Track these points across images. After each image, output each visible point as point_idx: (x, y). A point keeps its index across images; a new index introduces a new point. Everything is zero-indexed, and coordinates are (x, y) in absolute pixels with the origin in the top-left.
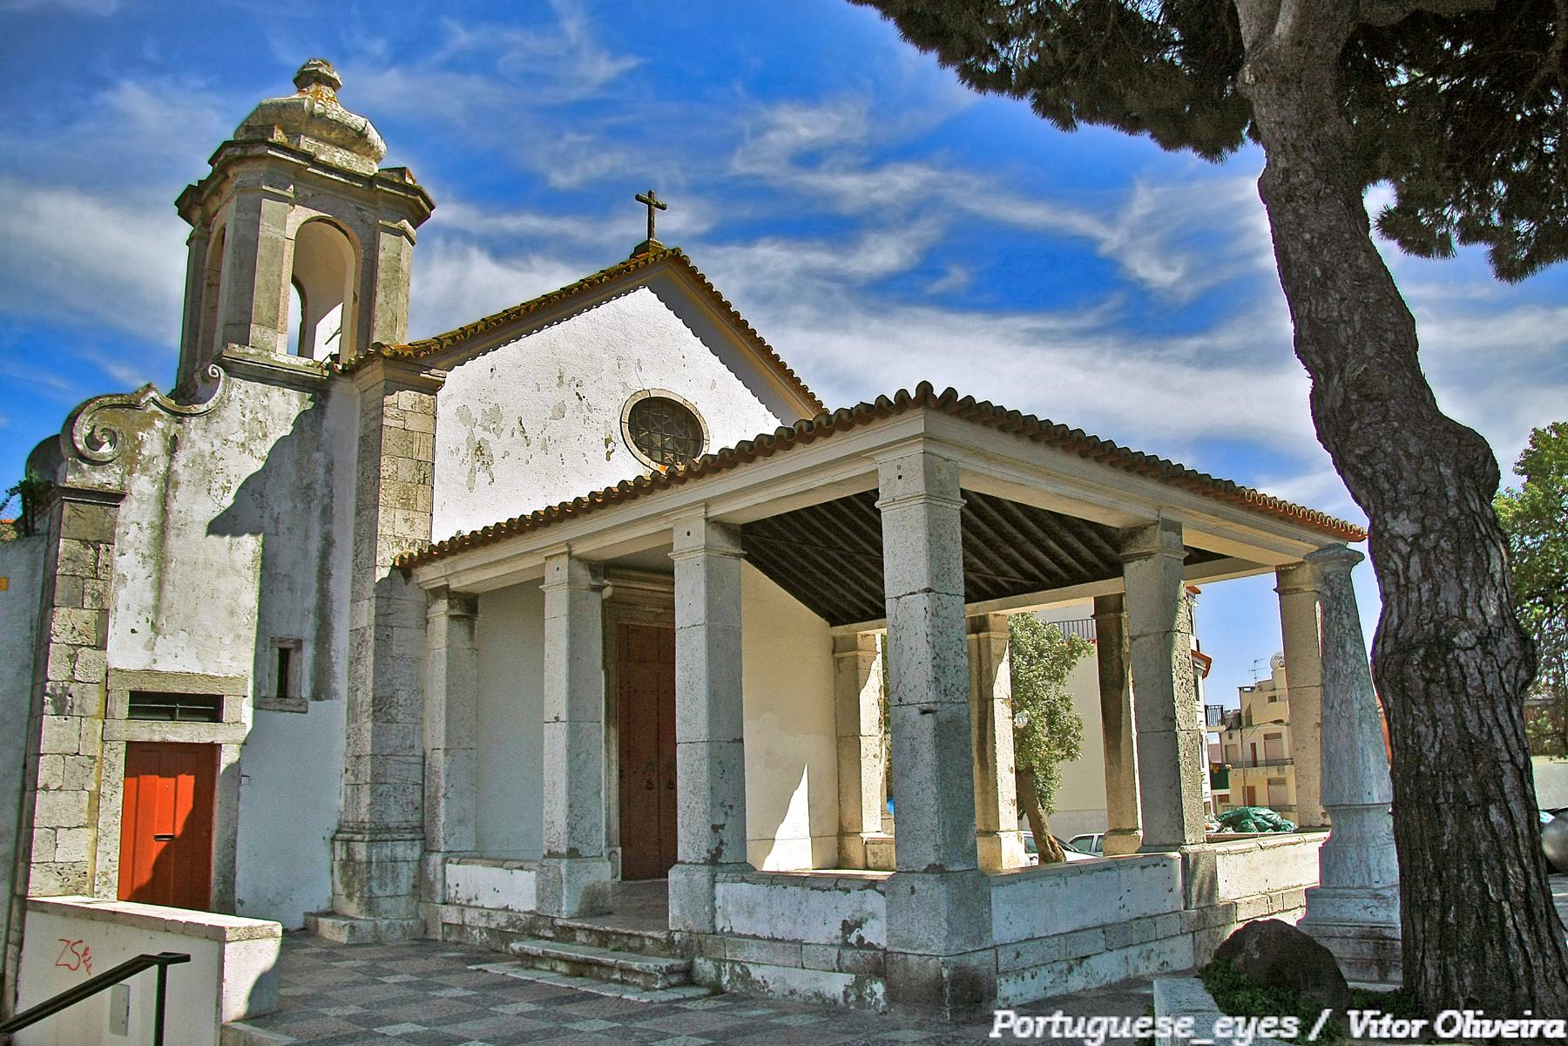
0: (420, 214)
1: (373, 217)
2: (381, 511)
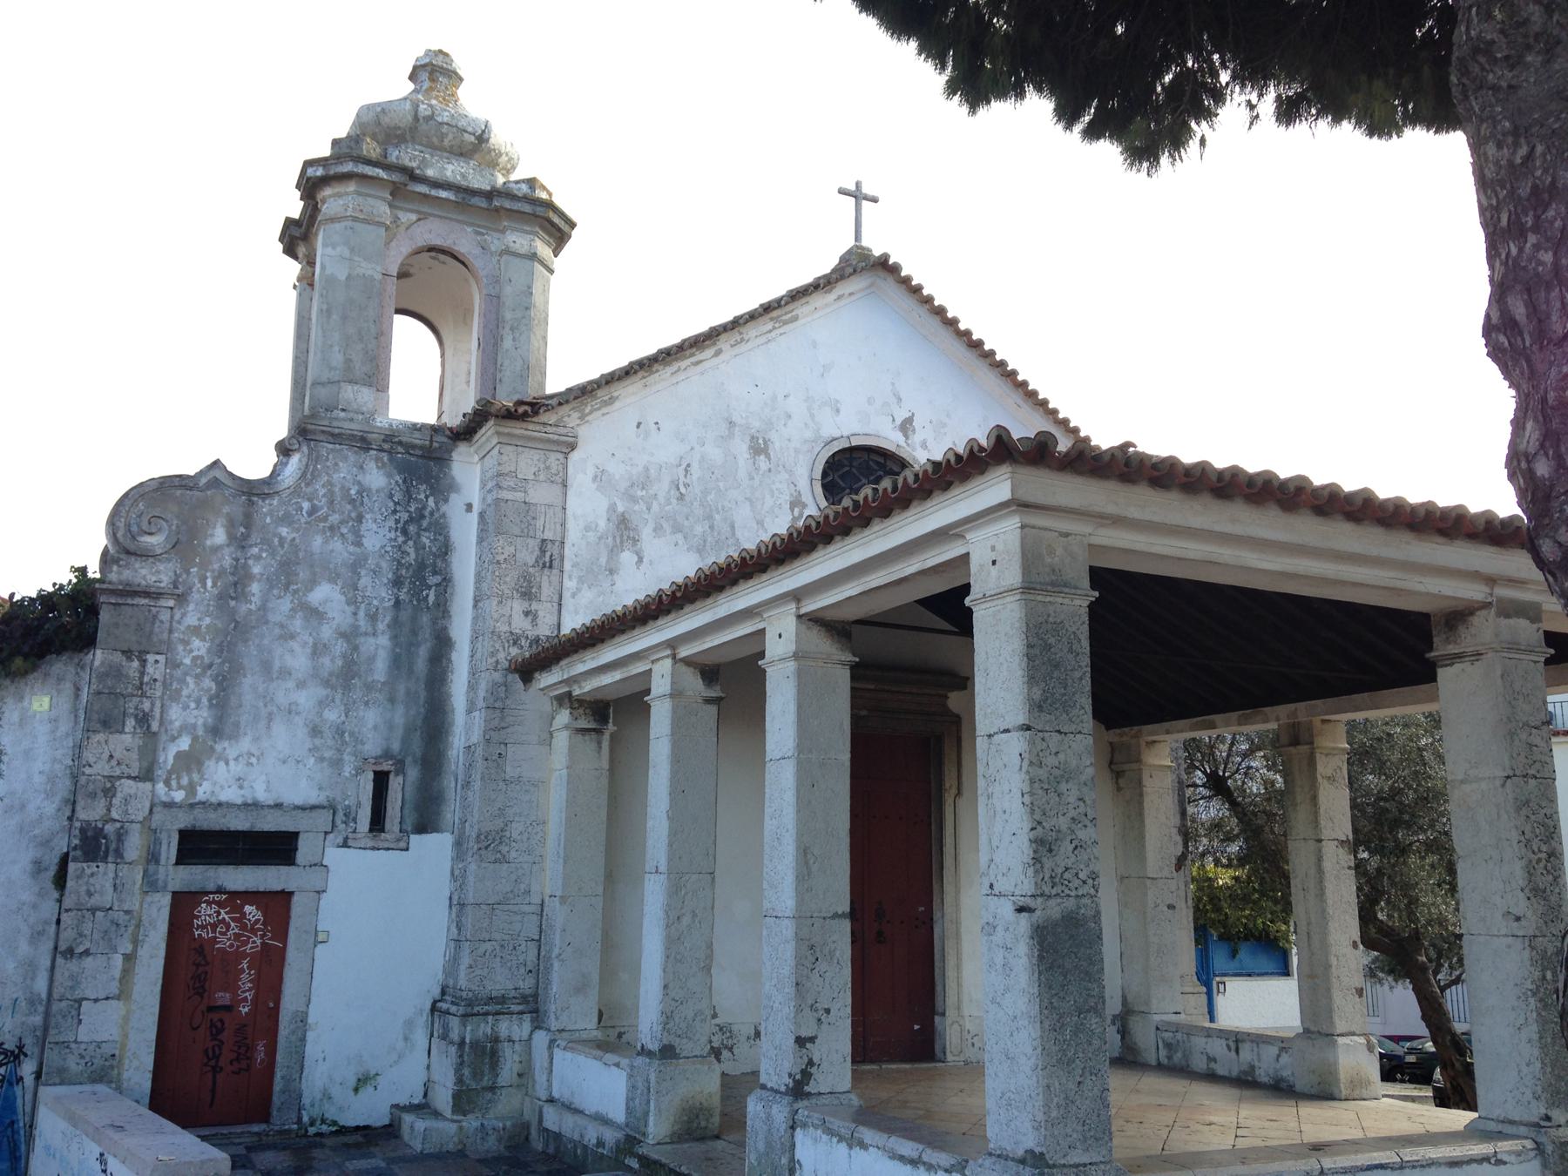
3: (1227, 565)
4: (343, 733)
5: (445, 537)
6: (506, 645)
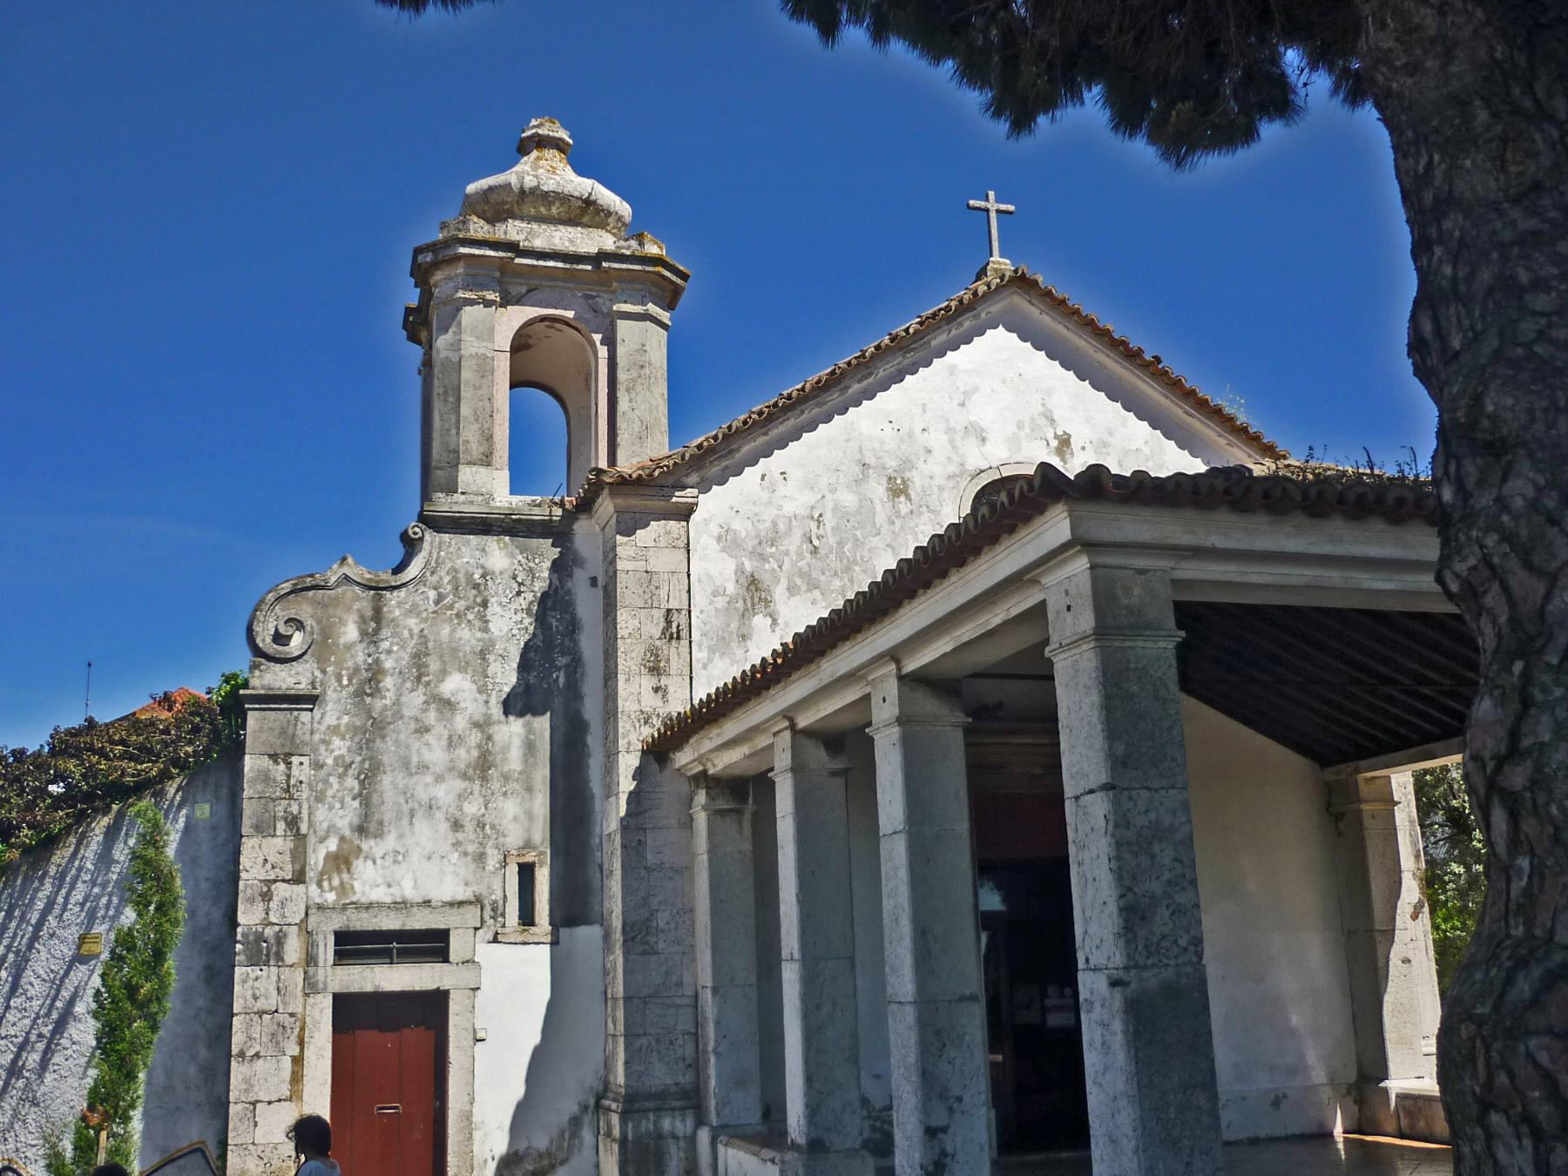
0: (672, 287)
1: (608, 303)
3: (1334, 588)
4: (484, 825)
5: (571, 616)
6: (638, 725)
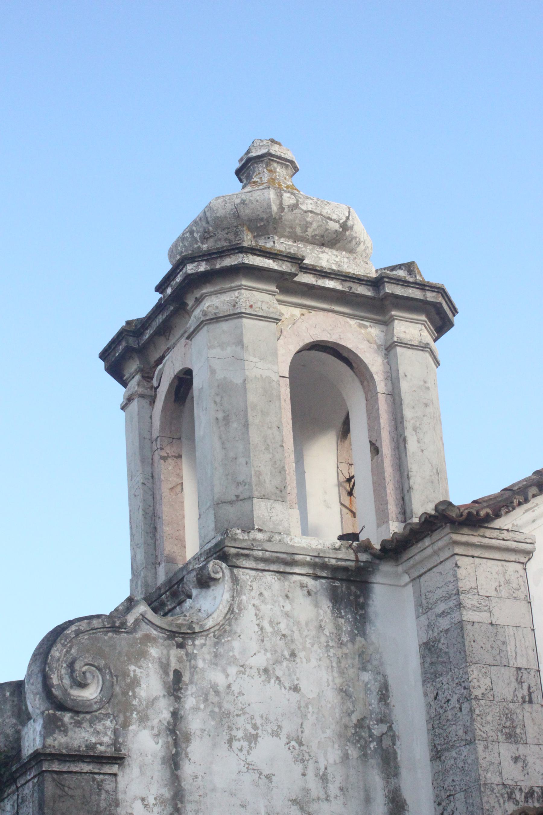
2: (480, 748)
6: (501, 801)
